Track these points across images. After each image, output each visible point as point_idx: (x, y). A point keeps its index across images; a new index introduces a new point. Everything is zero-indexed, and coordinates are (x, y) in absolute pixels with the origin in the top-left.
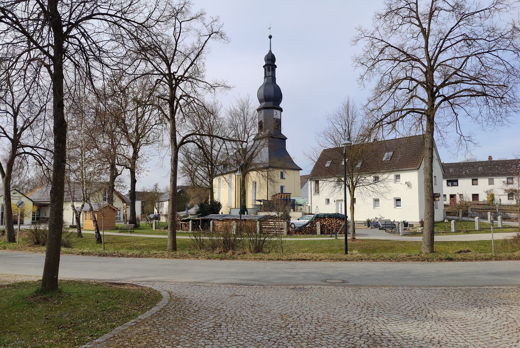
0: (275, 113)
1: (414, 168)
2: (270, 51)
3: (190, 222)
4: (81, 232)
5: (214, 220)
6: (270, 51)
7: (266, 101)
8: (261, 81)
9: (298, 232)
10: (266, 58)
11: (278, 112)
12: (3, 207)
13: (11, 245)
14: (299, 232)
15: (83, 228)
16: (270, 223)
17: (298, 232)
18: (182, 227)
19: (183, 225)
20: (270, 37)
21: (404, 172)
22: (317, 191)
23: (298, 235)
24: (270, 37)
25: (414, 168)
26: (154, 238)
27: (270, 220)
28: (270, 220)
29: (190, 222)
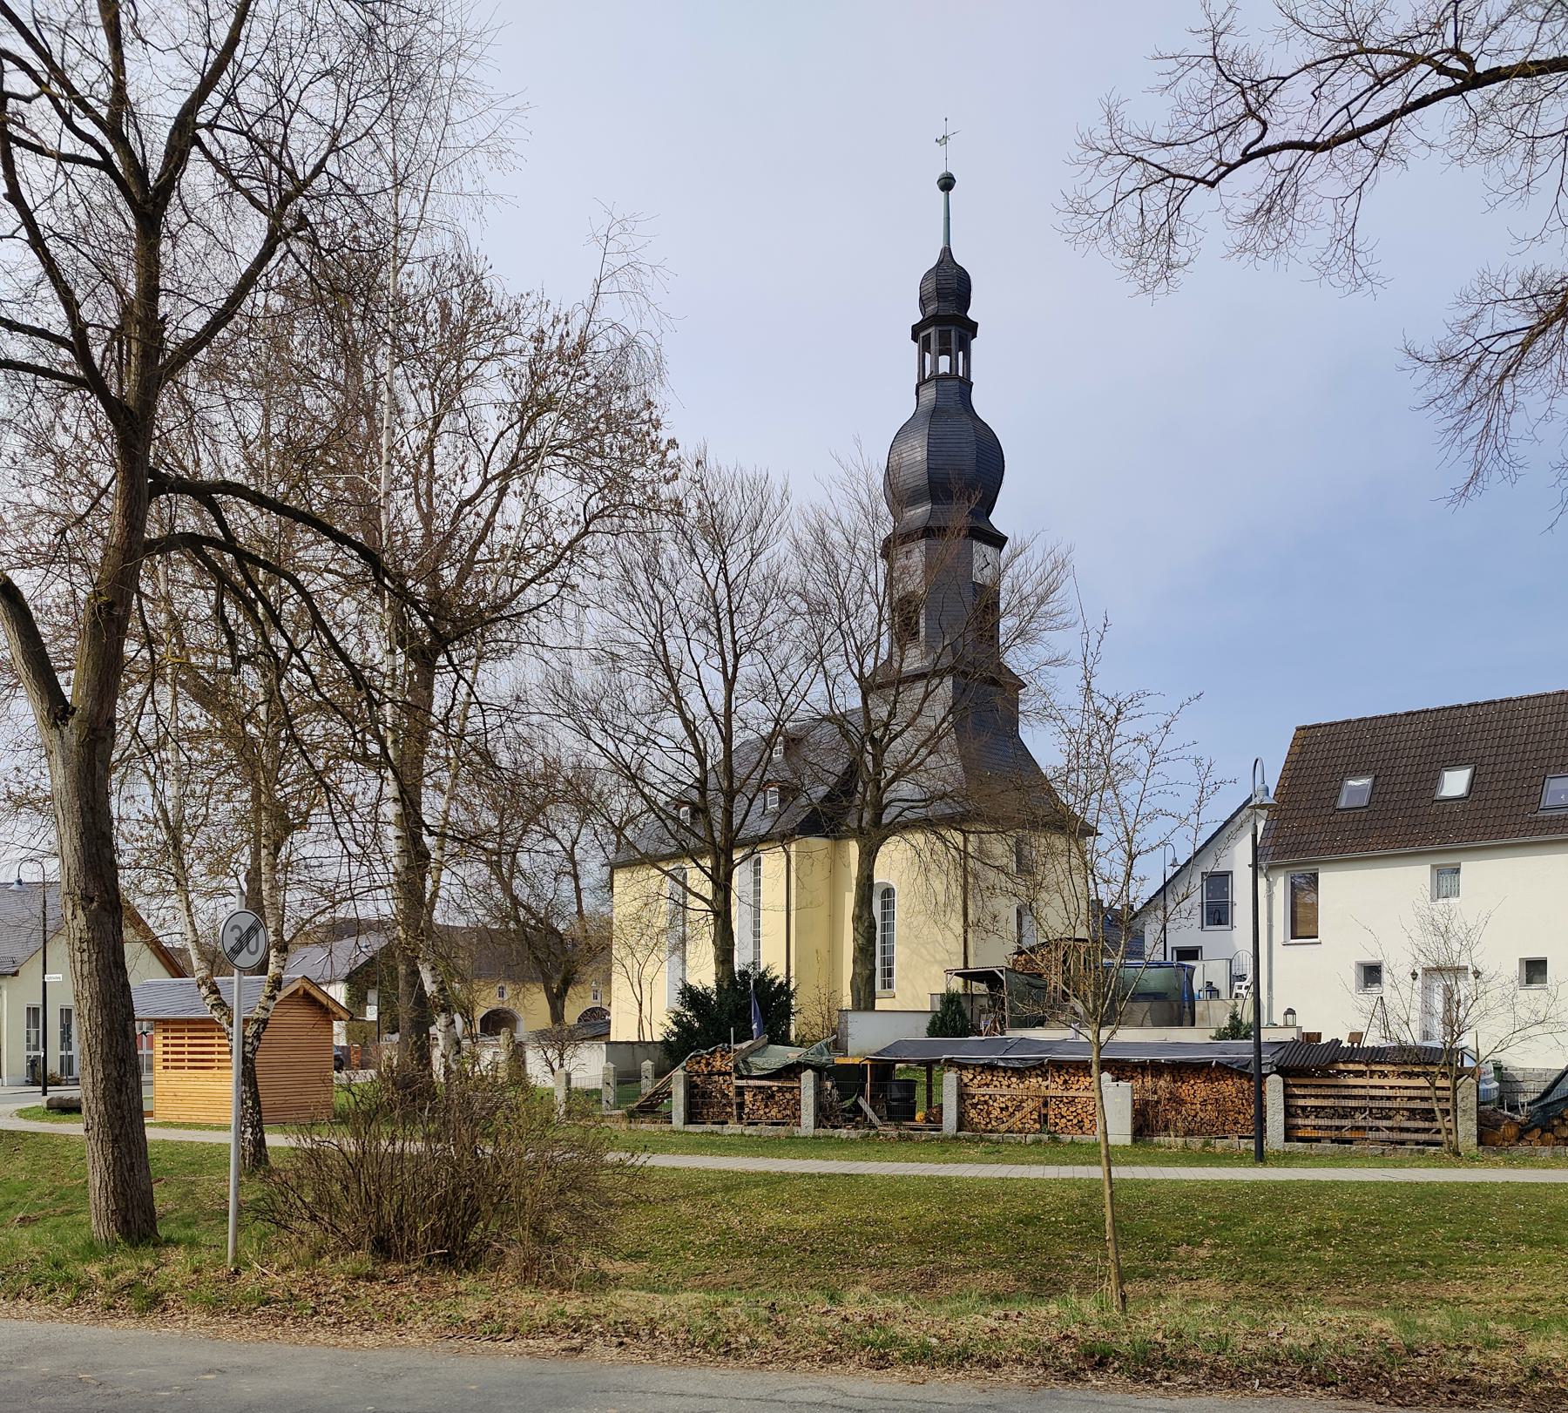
0: (978, 562)
1: (1407, 850)
2: (947, 252)
3: (808, 1077)
4: (263, 1140)
5: (962, 1066)
6: (947, 252)
7: (934, 499)
8: (901, 403)
9: (1537, 1132)
10: (931, 286)
11: (989, 551)
12: (888, 985)
13: (129, 1266)
14: (1544, 1131)
15: (151, 1114)
16: (1352, 1081)
17: (1537, 1132)
18: (741, 1106)
19: (748, 1097)
20: (947, 183)
21: (1483, 854)
22: (1303, 925)
23: (1546, 1152)
24: (947, 183)
25: (1407, 850)
26: (784, 1177)
27: (1351, 1067)
28: (1351, 1067)
29: (808, 1077)
